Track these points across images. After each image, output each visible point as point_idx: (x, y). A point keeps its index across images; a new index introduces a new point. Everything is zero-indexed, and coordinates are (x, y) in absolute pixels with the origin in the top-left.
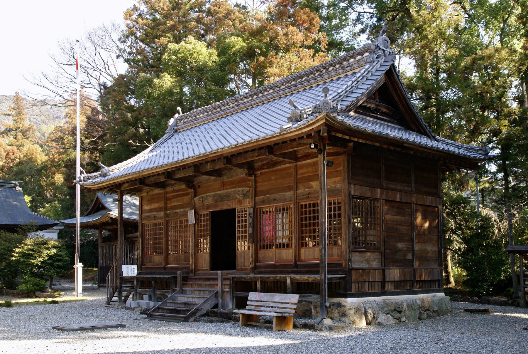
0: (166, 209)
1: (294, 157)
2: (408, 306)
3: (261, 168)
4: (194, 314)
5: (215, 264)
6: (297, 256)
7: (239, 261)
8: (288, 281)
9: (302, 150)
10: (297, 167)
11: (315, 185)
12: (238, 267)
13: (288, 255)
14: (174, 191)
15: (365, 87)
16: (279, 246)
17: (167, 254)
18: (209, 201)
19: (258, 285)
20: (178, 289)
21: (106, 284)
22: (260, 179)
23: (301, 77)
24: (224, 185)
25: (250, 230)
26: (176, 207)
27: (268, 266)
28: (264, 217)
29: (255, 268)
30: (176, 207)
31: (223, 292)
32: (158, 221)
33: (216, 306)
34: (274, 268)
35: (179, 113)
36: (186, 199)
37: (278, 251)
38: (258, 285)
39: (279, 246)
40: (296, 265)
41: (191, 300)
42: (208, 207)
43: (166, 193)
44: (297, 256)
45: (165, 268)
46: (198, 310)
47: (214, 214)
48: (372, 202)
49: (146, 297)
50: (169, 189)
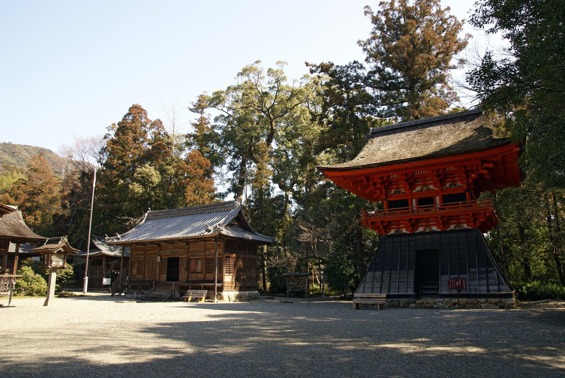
0: (145, 254)
2: (244, 295)
3: (191, 243)
5: (169, 279)
6: (205, 277)
7: (180, 278)
8: (202, 286)
10: (206, 244)
11: (213, 251)
12: (179, 281)
13: (201, 276)
14: (150, 247)
16: (198, 273)
17: (145, 274)
19: (190, 287)
20: (153, 289)
21: (89, 290)
23: (207, 207)
24: (174, 248)
25: (186, 266)
29: (187, 281)
31: (175, 290)
33: (172, 296)
35: (149, 210)
36: (156, 251)
37: (197, 274)
38: (190, 287)
39: (198, 273)
40: (204, 280)
42: (166, 256)
43: (146, 248)
44: (205, 277)
46: (165, 297)
49: (135, 293)
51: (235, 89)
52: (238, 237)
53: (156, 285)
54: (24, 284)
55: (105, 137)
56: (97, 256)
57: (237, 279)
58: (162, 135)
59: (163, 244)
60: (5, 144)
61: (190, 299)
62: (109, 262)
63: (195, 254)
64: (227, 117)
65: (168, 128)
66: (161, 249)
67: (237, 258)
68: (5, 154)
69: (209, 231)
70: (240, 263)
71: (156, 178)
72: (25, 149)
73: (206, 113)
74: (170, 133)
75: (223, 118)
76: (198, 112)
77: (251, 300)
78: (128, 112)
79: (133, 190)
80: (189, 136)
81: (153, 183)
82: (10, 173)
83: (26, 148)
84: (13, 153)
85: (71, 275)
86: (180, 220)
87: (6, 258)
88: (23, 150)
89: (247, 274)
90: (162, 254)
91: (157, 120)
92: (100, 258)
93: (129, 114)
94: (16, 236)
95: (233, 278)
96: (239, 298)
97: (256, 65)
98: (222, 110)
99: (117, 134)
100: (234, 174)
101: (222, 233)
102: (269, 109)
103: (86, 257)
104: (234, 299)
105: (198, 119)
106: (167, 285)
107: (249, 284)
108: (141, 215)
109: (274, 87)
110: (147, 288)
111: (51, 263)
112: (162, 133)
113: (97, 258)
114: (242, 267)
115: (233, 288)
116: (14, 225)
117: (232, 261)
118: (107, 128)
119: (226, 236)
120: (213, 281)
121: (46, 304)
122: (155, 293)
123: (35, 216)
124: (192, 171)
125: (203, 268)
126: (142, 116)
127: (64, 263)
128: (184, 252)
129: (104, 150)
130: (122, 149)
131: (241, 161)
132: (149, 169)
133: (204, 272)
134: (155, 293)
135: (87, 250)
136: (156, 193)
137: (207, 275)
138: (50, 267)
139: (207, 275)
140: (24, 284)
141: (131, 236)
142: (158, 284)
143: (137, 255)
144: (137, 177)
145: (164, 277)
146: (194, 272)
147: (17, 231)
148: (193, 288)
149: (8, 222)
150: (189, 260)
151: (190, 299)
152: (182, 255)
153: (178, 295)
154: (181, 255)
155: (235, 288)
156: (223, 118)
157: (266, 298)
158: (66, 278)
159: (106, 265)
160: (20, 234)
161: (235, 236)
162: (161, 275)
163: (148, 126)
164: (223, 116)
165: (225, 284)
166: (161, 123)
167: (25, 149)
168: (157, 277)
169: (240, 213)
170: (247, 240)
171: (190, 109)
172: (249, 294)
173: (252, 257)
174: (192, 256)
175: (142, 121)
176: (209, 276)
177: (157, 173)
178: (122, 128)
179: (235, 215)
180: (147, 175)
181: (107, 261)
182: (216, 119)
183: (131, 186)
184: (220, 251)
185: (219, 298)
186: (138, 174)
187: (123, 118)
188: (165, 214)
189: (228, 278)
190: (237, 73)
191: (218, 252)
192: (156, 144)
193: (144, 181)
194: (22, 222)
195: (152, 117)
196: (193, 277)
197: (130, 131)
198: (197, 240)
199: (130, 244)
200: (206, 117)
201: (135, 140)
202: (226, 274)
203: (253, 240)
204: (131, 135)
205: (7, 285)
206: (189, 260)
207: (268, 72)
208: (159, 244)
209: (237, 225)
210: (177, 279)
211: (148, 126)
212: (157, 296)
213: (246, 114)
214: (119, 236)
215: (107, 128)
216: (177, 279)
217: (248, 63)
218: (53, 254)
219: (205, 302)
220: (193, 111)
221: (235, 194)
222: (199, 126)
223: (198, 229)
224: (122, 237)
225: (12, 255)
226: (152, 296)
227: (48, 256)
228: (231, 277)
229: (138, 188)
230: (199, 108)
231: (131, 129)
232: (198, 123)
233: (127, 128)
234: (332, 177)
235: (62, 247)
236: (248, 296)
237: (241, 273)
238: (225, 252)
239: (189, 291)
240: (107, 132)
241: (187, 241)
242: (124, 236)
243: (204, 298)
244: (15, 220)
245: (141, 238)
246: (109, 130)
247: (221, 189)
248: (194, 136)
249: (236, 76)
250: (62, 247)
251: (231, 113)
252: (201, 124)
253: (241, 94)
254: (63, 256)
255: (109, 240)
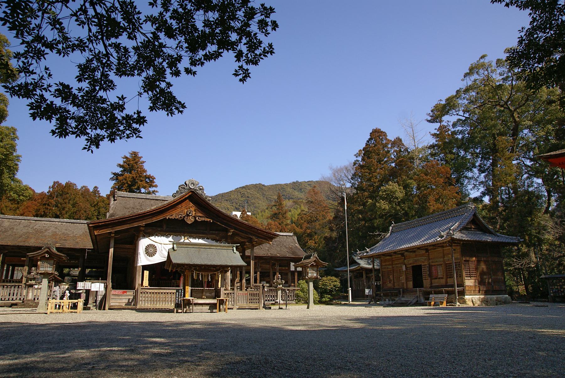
1: (443, 247)
4: (410, 304)
5: (415, 286)
6: (446, 282)
7: (425, 285)
9: (445, 245)
10: (443, 250)
13: (443, 282)
14: (396, 257)
15: (465, 222)
16: (439, 278)
18: (411, 262)
19: (433, 292)
22: (430, 254)
26: (396, 264)
27: (435, 286)
28: (433, 267)
30: (396, 264)
32: (389, 269)
33: (417, 301)
34: (438, 287)
36: (401, 261)
38: (433, 292)
39: (439, 278)
41: (407, 299)
42: (410, 264)
44: (446, 282)
45: (393, 288)
47: (413, 267)
48: (11, 267)
50: (393, 257)
51: (467, 90)
52: (473, 240)
53: (403, 292)
54: (301, 294)
55: (355, 164)
56: (357, 270)
57: (481, 282)
58: (403, 152)
59: (406, 253)
60: (294, 183)
61: (432, 303)
62: (368, 274)
63: (435, 260)
64: (465, 120)
65: (408, 143)
66: (405, 258)
67: (479, 262)
68: (295, 191)
69: (442, 237)
70: (483, 266)
71: (400, 194)
72: (309, 185)
73: (445, 121)
74: (411, 148)
75: (461, 122)
76: (437, 122)
77: (500, 304)
78: (369, 137)
79: (380, 207)
80: (432, 147)
81: (397, 198)
82: (299, 206)
83: (309, 183)
84: (301, 189)
85: (338, 287)
86: (419, 229)
87: (290, 274)
88: (307, 185)
89: (492, 277)
90: (406, 263)
91: (397, 138)
92: (361, 271)
93: (371, 139)
94: (293, 256)
95: (475, 282)
96: (483, 301)
97: (482, 61)
98: (457, 114)
99: (363, 160)
100: (485, 177)
101: (453, 238)
102: (508, 101)
103: (347, 271)
104: (479, 302)
105: (437, 128)
106: (413, 292)
107: (497, 287)
108: (386, 230)
109: (508, 77)
110: (396, 296)
111: (308, 274)
112: (402, 150)
113: (358, 271)
114: (485, 270)
115: (477, 292)
116: (291, 248)
117: (472, 266)
118: (355, 155)
119: (459, 240)
120: (453, 286)
121: (308, 308)
122: (403, 299)
123: (314, 240)
124: (432, 181)
125: (443, 273)
126: (382, 138)
127: (317, 274)
128: (425, 260)
129: (355, 175)
130: (369, 171)
131: (491, 161)
132: (393, 186)
133: (445, 277)
134: (403, 299)
135: (347, 266)
136: (401, 207)
137: (448, 279)
138: (307, 278)
139: (448, 279)
140: (301, 294)
141: (380, 248)
142: (406, 291)
143: (386, 265)
144: (383, 195)
145: (411, 284)
146: (436, 278)
147: (293, 253)
148: (436, 293)
149: (287, 246)
150: (430, 267)
151: (432, 303)
152: (422, 261)
153: (423, 301)
154: (423, 262)
155: (479, 292)
156: (461, 122)
157: (519, 302)
158: (335, 289)
159: (367, 277)
160: (296, 255)
161: (469, 239)
162: (408, 282)
163: (390, 146)
164: (461, 120)
165: (467, 288)
166: (401, 140)
167: (309, 185)
168: (405, 285)
169: (475, 215)
170: (486, 243)
171: (428, 121)
172: (497, 298)
173: (496, 259)
174: (432, 262)
175: (383, 142)
176: (450, 281)
177: (400, 189)
178: (367, 152)
179: (471, 217)
180: (391, 192)
181: (366, 274)
182: (454, 125)
183: (378, 204)
184: (457, 255)
185: (461, 302)
186: (382, 192)
187: (366, 143)
188: (406, 226)
189: (469, 282)
190: (464, 74)
191: (455, 255)
192: (398, 161)
193: (389, 197)
194: (297, 245)
195: (391, 137)
196: (436, 282)
197: (373, 154)
198: (435, 246)
199: (378, 256)
200: (446, 124)
201: (379, 161)
202: (466, 278)
203: (492, 241)
204: (375, 157)
205: (292, 296)
206: (430, 267)
207: (496, 64)
208: (402, 253)
209: (474, 229)
210: (422, 286)
211: (390, 146)
212: (404, 302)
213: (483, 112)
214: (368, 250)
215: (355, 155)
216: (422, 286)
217: (474, 59)
218: (308, 267)
219: (447, 305)
220: (431, 122)
221: (491, 196)
222: (440, 134)
223: (434, 236)
224: (370, 250)
225: (293, 273)
226: (400, 302)
227: (305, 269)
228: (473, 281)
229: (384, 205)
230: (436, 117)
231: (374, 152)
232: (438, 133)
233: (371, 152)
234: (560, 164)
235: (314, 261)
236: (496, 300)
237: (485, 277)
238: (462, 256)
239: (431, 296)
240: (356, 159)
241: (426, 248)
242: (373, 249)
243: (445, 302)
244: (292, 244)
245: (386, 250)
246: (357, 157)
247: (475, 194)
248: (436, 145)
249: (463, 77)
250: (314, 261)
251: (467, 115)
252: (441, 133)
253: (474, 94)
254: (316, 269)
255: (360, 254)
